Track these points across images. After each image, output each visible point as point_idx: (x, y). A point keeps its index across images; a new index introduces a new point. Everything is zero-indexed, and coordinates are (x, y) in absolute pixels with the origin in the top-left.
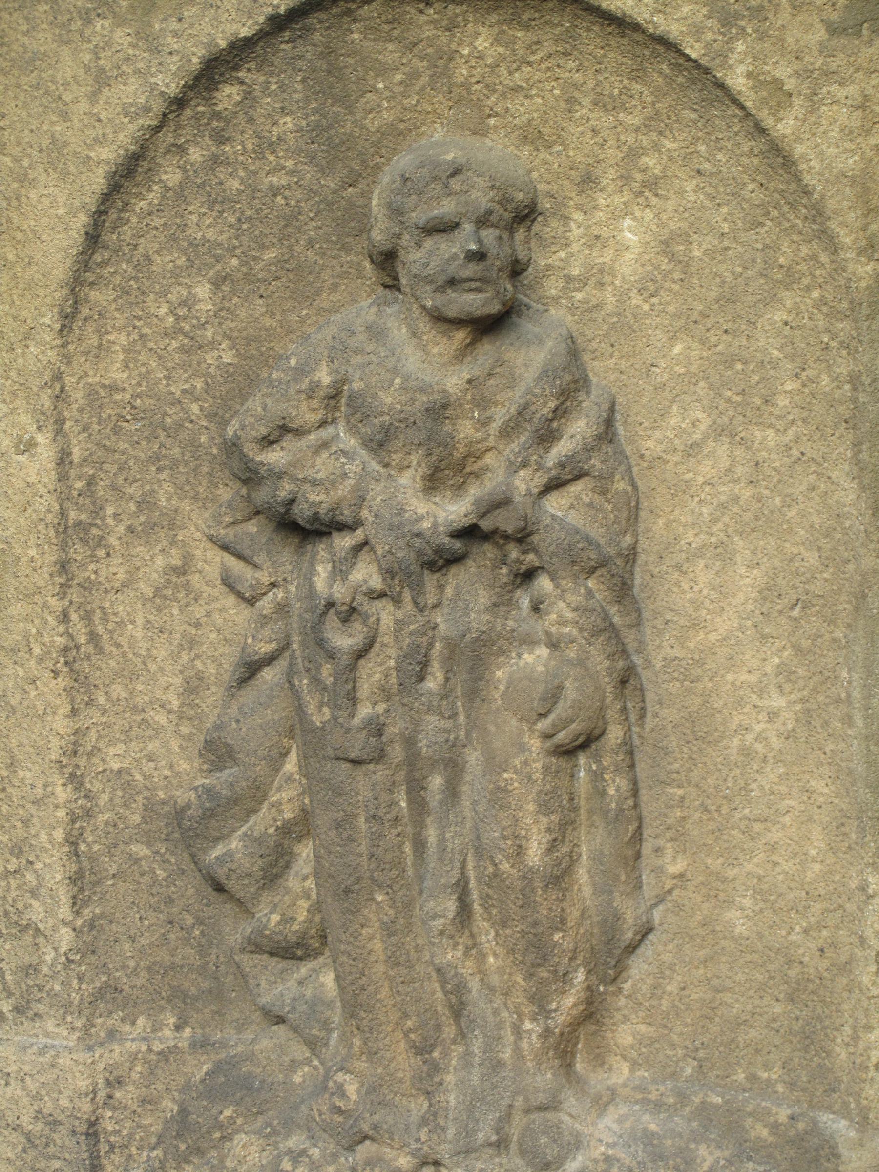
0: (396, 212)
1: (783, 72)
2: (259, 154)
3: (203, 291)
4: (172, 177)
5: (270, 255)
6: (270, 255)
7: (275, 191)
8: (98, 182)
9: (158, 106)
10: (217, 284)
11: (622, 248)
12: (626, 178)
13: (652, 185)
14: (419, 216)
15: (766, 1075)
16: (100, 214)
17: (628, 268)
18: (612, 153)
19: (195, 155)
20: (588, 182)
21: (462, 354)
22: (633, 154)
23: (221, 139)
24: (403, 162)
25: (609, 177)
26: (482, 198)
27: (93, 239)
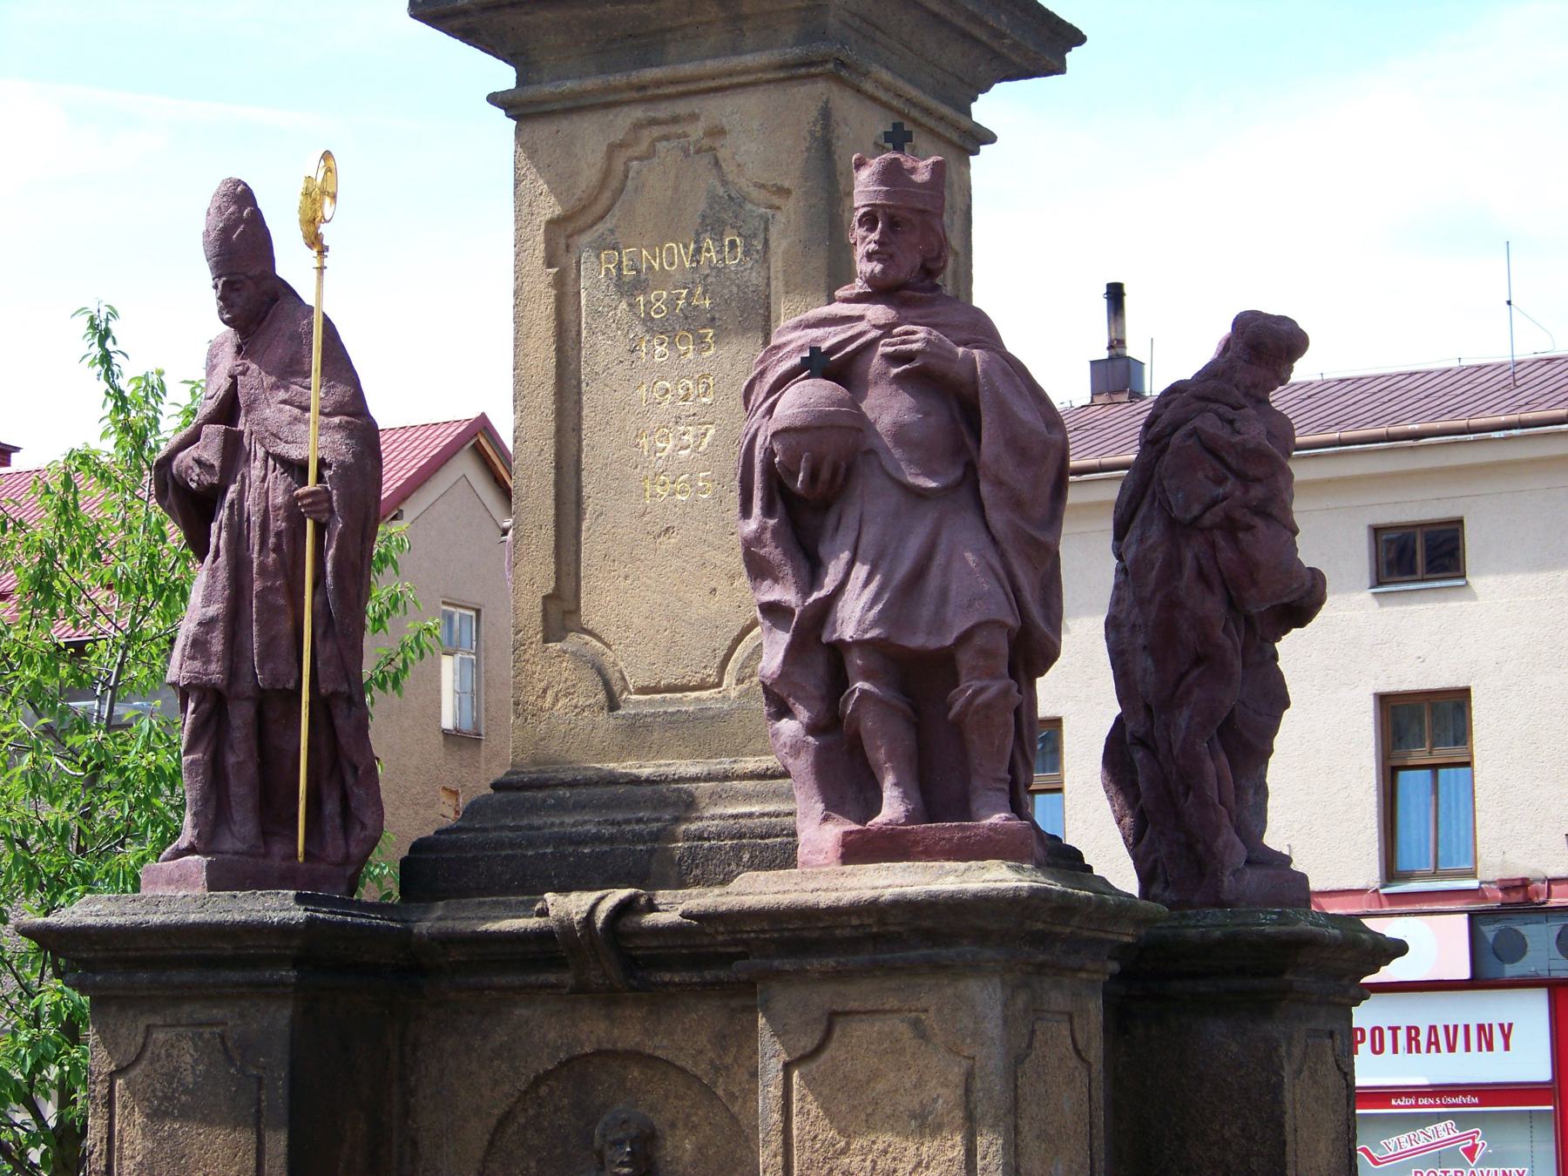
0: (604, 1136)
1: (736, 1090)
2: (555, 1112)
3: (533, 1164)
4: (522, 1120)
5: (558, 1151)
6: (558, 1151)
7: (561, 1127)
8: (494, 1121)
9: (517, 1094)
10: (538, 1162)
11: (685, 1150)
12: (686, 1125)
13: (695, 1127)
14: (610, 1138)
15: (45, 720)
16: (493, 1135)
17: (687, 1158)
18: (681, 1116)
19: (531, 1112)
20: (673, 1126)
21: (1249, 528)
22: (688, 1116)
23: (540, 1106)
24: (606, 1118)
25: (680, 1125)
26: (633, 1132)
27: (491, 1143)
